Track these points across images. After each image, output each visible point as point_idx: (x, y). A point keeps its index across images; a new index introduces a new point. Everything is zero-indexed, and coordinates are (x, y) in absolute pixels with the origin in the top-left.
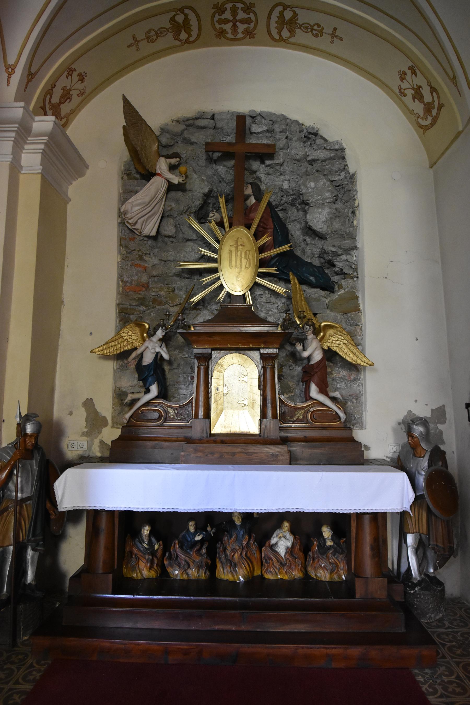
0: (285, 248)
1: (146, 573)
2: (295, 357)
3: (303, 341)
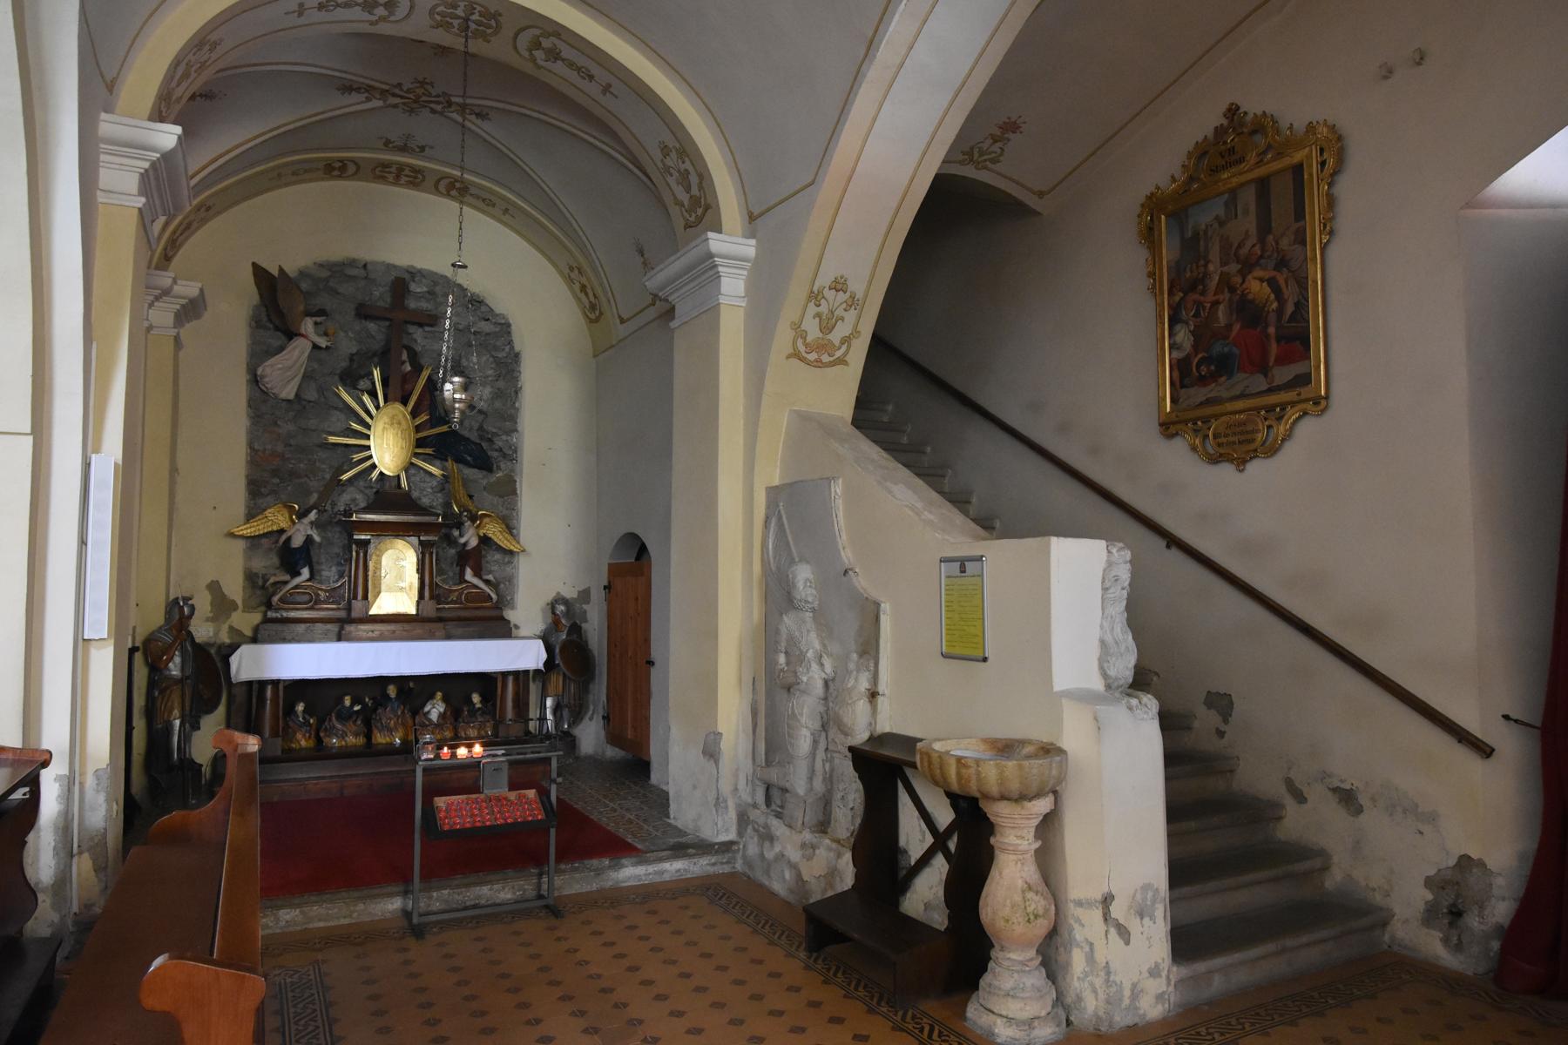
0: (445, 428)
1: (303, 743)
2: (451, 541)
3: (459, 525)
